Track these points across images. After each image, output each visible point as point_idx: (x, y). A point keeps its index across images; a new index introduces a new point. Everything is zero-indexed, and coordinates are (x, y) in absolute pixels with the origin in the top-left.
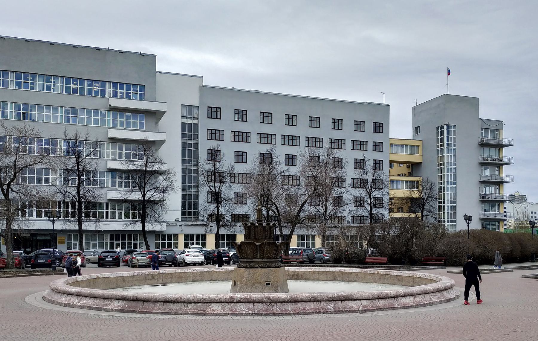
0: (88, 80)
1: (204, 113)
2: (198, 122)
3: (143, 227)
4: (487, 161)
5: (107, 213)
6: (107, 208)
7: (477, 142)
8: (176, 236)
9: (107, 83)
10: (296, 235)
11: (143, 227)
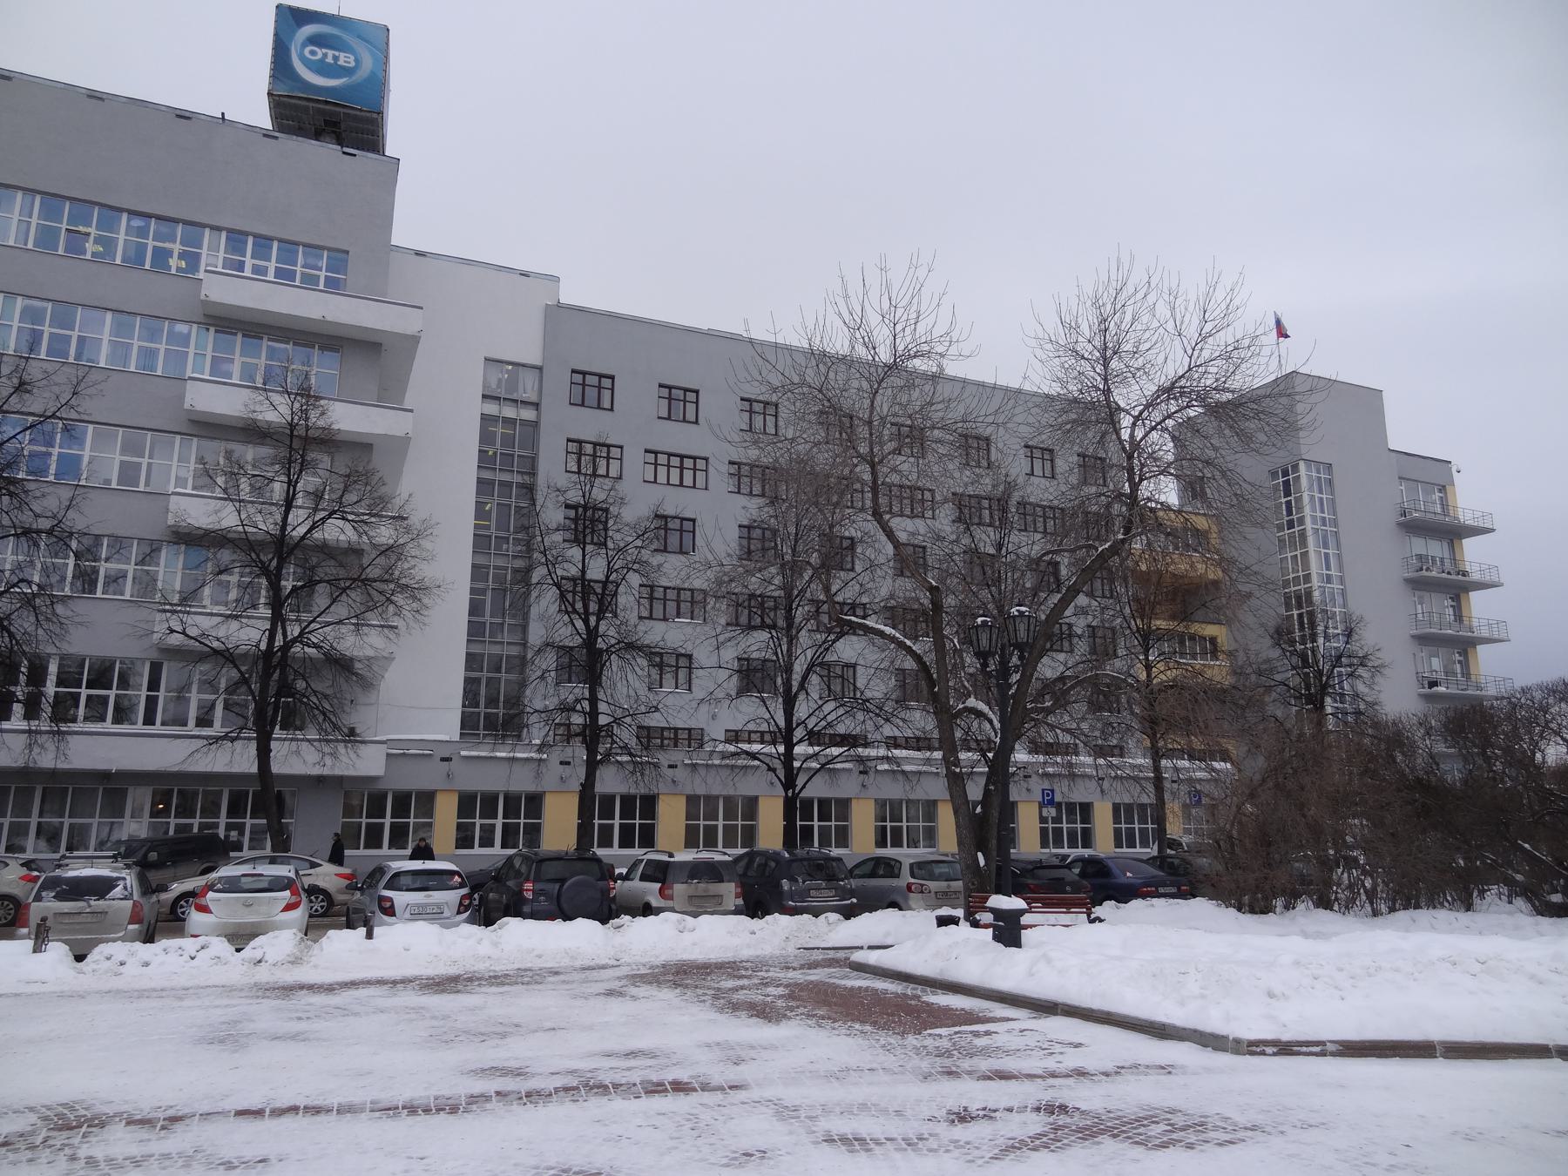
0: (133, 213)
1: (559, 387)
2: (539, 416)
3: (264, 754)
4: (1428, 574)
5: (151, 703)
6: (154, 685)
7: (1392, 517)
8: (427, 799)
9: (207, 231)
10: (683, 800)
11: (264, 754)
